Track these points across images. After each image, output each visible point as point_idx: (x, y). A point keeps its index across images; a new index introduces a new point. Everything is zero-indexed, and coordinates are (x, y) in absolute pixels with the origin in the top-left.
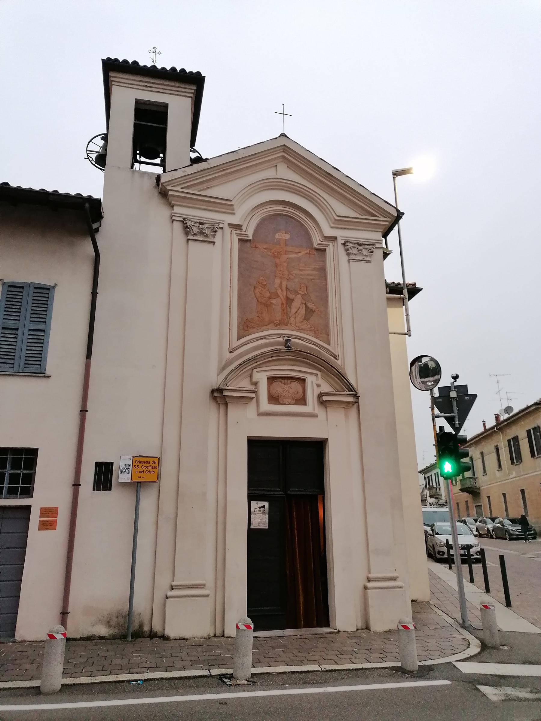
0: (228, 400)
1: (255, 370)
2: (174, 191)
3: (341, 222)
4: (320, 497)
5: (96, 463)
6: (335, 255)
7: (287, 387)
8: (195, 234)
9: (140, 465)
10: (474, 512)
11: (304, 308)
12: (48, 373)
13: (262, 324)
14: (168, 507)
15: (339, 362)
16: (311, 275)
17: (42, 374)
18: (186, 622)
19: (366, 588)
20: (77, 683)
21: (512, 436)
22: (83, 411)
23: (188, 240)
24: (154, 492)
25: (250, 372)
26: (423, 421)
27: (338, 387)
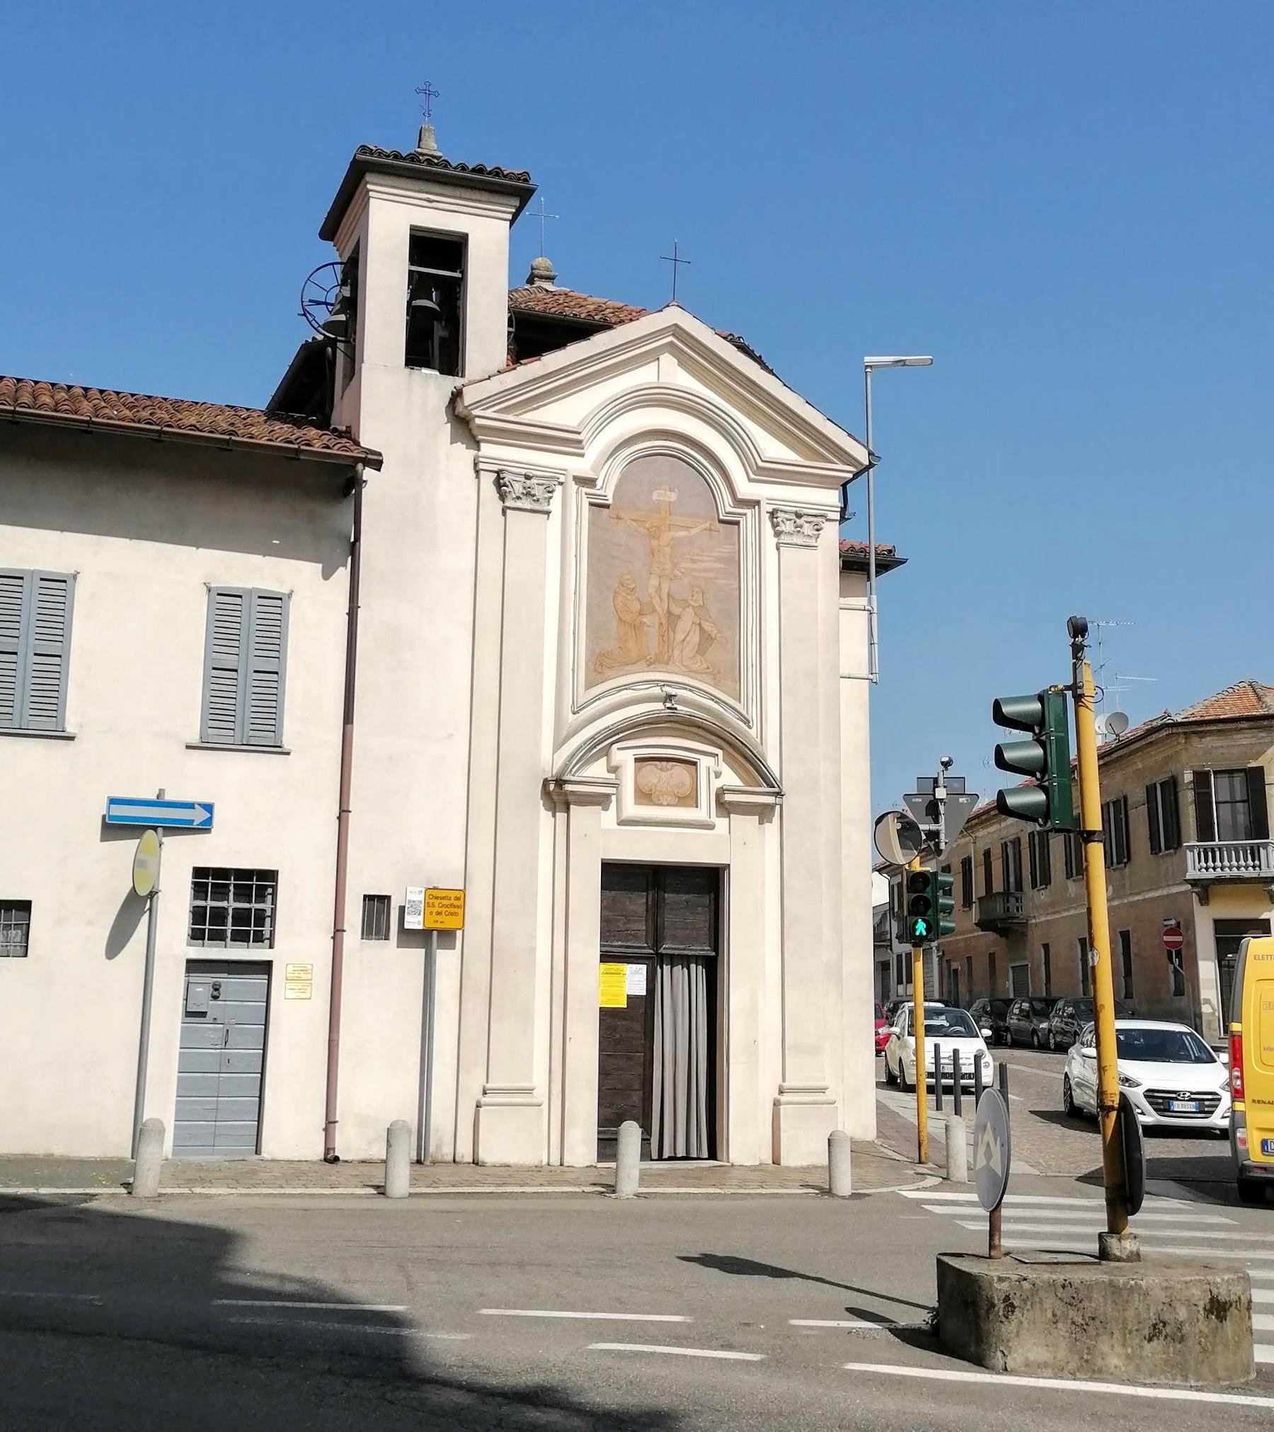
1: (615, 747)
2: (484, 417)
7: (665, 775)
12: (287, 742)
14: (478, 970)
16: (712, 570)
19: (776, 1104)
20: (512, 1159)
22: (343, 812)
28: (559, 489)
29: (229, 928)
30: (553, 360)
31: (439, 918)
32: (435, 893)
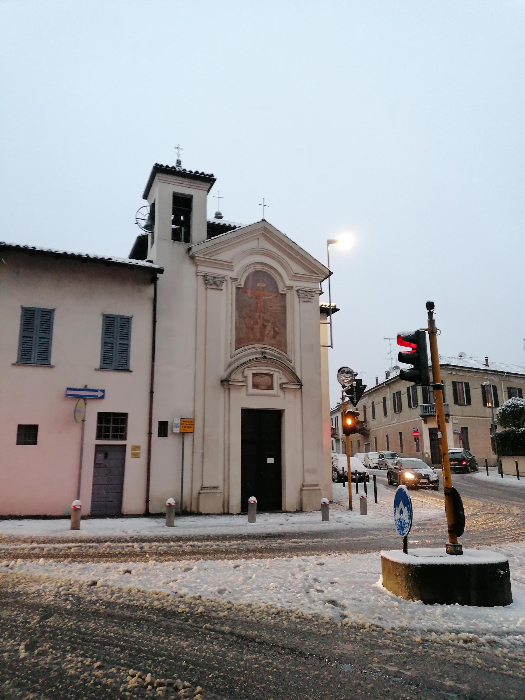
0: (231, 387)
2: (199, 257)
5: (159, 422)
6: (292, 299)
8: (211, 285)
11: (273, 331)
15: (292, 364)
19: (301, 490)
21: (397, 391)
22: (152, 392)
23: (207, 288)
25: (242, 371)
28: (225, 282)
29: (111, 433)
31: (185, 429)
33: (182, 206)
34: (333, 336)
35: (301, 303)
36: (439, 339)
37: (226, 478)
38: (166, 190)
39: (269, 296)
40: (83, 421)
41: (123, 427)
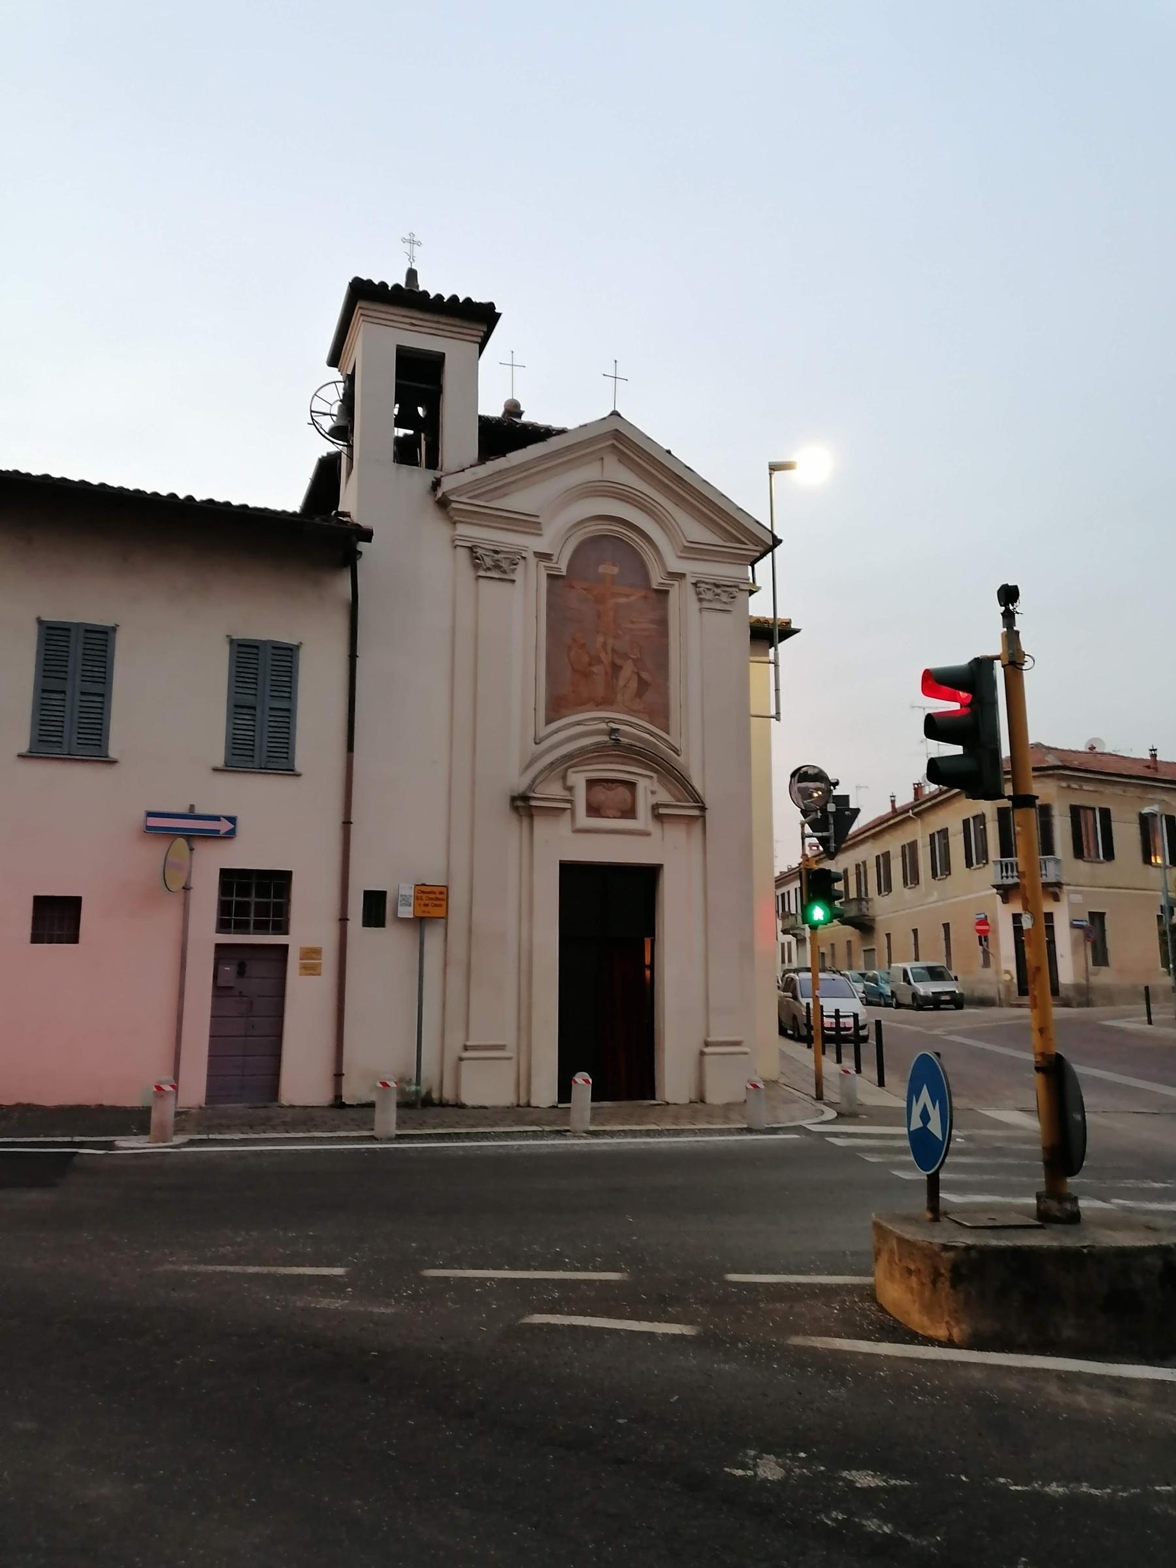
1: (570, 771)
2: (461, 501)
3: (693, 551)
4: (648, 941)
6: (681, 601)
7: (611, 794)
8: (489, 569)
9: (424, 896)
10: (860, 961)
12: (298, 768)
13: (580, 703)
15: (681, 759)
17: (290, 771)
18: (485, 1087)
19: (702, 1054)
22: (347, 823)
24: (441, 930)
26: (788, 841)
27: (678, 795)
29: (252, 918)
30: (516, 457)
32: (423, 888)
33: (420, 380)
34: (781, 693)
35: (705, 613)
36: (1030, 678)
37: (524, 1022)
38: (382, 340)
39: (628, 596)
40: (187, 888)
41: (281, 904)
